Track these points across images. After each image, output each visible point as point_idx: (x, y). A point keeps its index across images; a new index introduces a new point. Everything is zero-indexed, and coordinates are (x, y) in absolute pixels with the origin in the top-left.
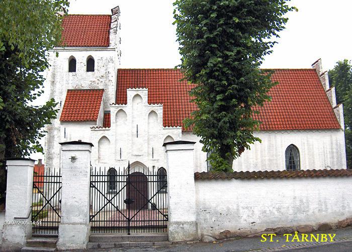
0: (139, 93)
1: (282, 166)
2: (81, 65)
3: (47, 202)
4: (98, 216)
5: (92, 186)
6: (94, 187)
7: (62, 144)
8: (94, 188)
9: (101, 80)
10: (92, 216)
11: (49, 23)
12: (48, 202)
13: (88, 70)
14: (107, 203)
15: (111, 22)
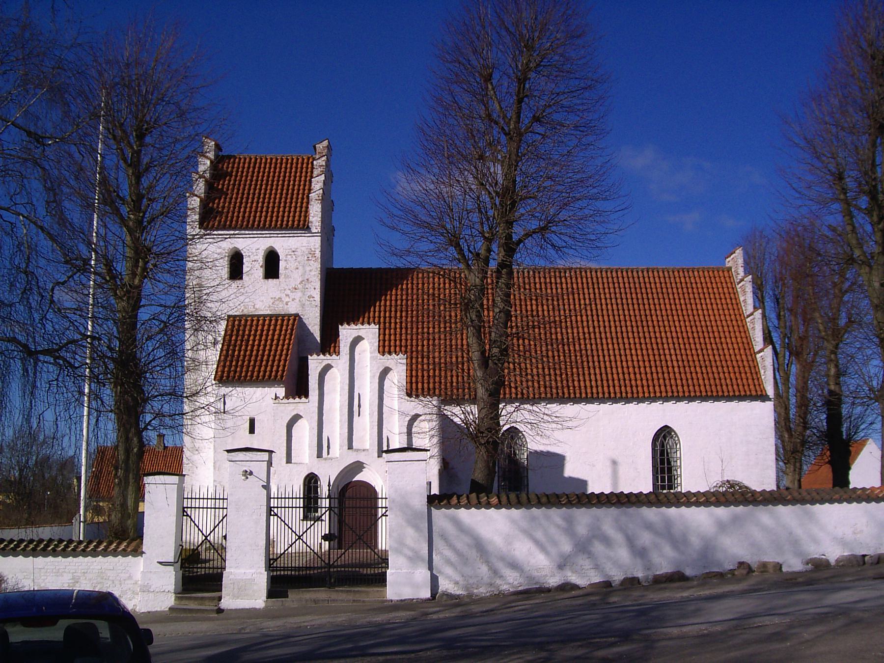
0: (362, 333)
1: (646, 487)
2: (253, 266)
3: (204, 538)
4: (282, 559)
5: (272, 513)
6: (276, 515)
7: (228, 451)
8: (276, 517)
9: (292, 295)
10: (273, 559)
11: (159, 77)
12: (206, 537)
13: (287, 463)
14: (296, 540)
15: (312, 177)
